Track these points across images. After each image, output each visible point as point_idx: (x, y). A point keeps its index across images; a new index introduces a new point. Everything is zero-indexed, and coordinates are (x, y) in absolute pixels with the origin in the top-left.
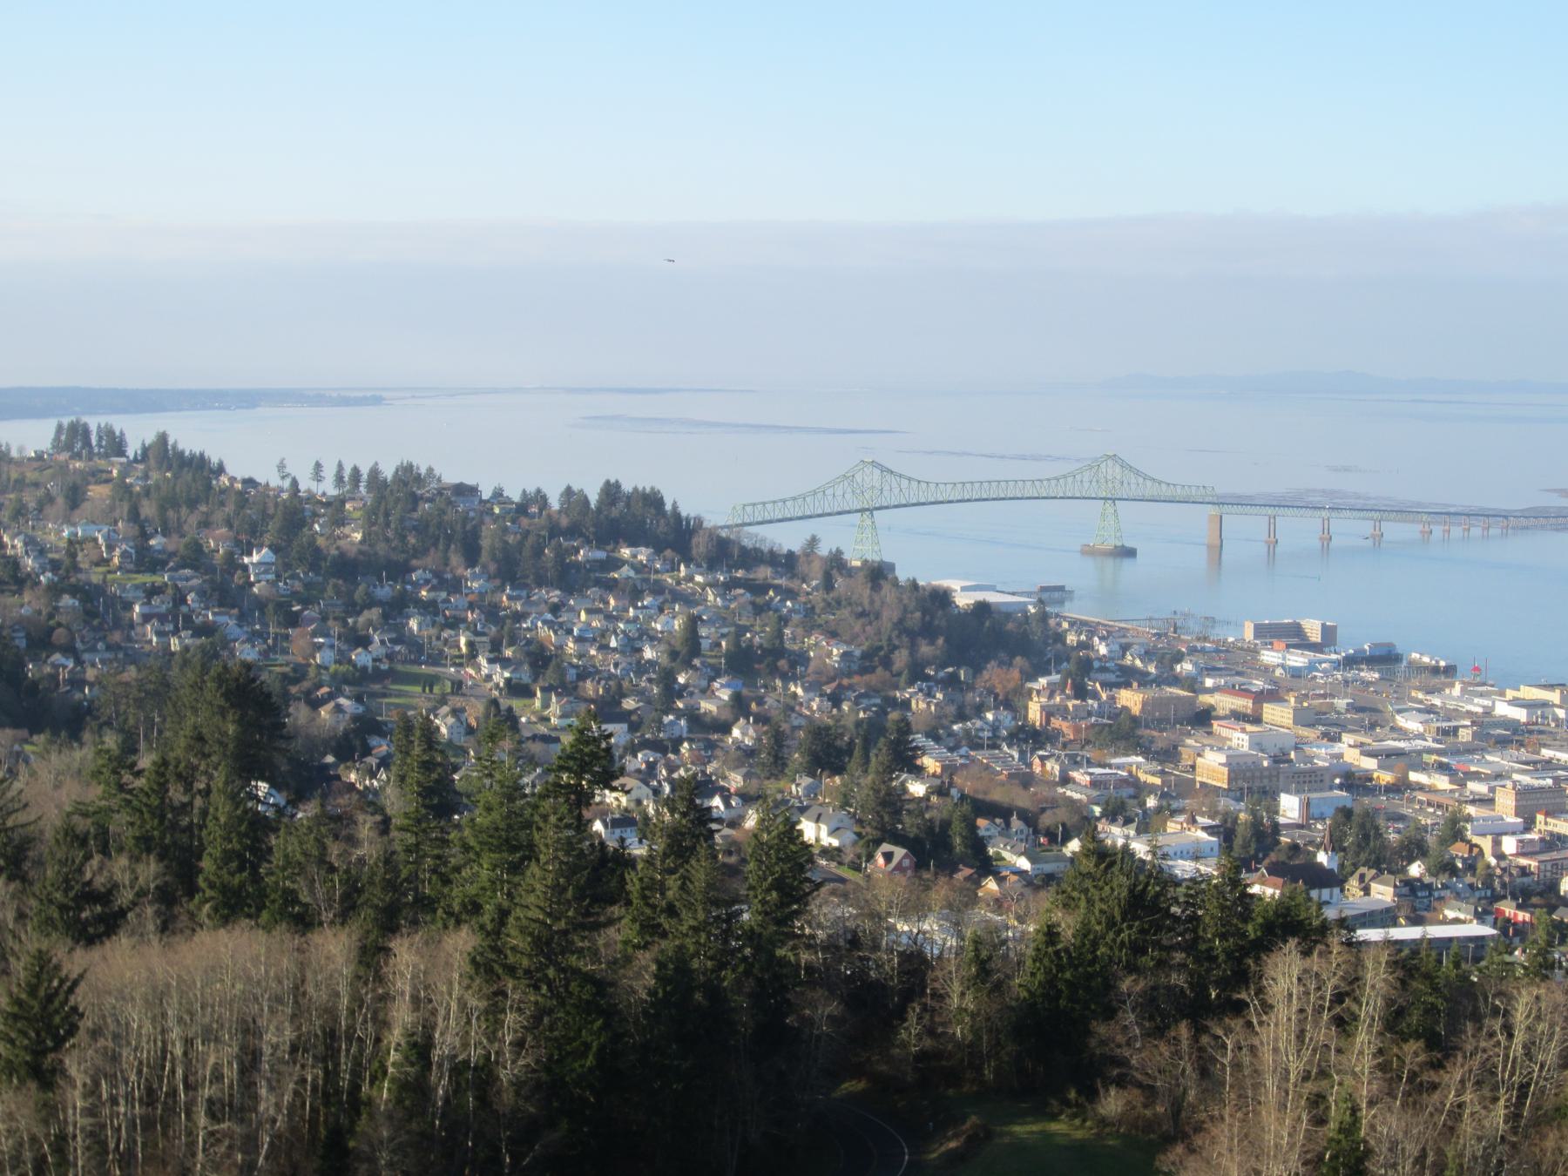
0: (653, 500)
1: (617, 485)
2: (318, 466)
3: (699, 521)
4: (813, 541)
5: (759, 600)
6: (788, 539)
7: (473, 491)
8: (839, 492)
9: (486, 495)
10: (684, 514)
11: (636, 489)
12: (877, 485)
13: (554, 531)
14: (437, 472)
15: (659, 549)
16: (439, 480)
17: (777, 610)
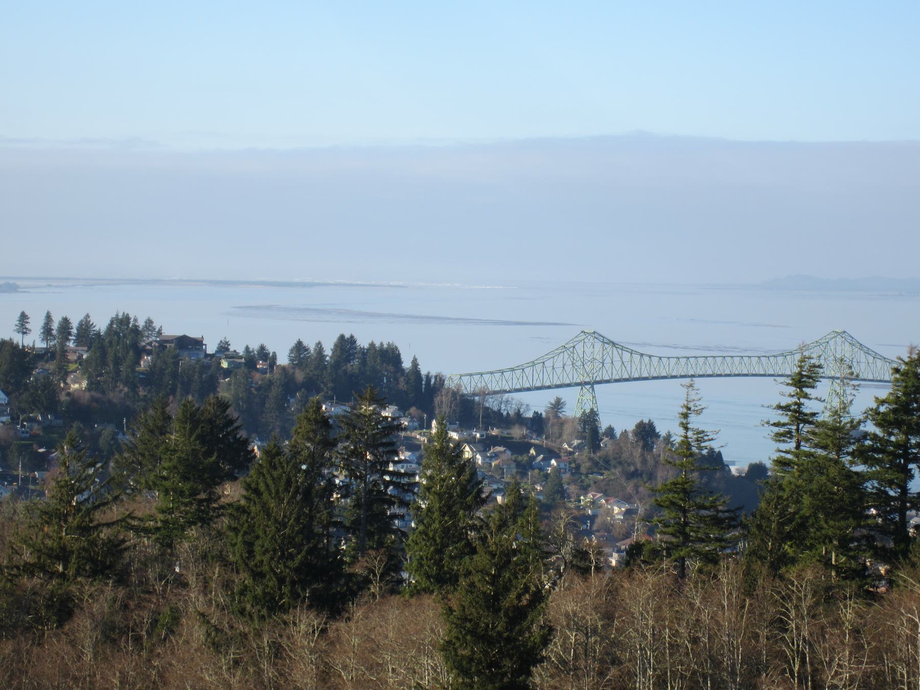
0: (389, 356)
1: (352, 341)
2: (24, 317)
3: (440, 380)
4: (558, 405)
5: (524, 458)
6: (536, 404)
7: (198, 344)
8: (559, 364)
9: (211, 348)
10: (424, 372)
11: (372, 345)
12: (599, 357)
13: (288, 384)
14: (157, 325)
15: (404, 408)
16: (159, 333)
17: (541, 469)
